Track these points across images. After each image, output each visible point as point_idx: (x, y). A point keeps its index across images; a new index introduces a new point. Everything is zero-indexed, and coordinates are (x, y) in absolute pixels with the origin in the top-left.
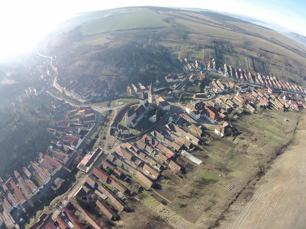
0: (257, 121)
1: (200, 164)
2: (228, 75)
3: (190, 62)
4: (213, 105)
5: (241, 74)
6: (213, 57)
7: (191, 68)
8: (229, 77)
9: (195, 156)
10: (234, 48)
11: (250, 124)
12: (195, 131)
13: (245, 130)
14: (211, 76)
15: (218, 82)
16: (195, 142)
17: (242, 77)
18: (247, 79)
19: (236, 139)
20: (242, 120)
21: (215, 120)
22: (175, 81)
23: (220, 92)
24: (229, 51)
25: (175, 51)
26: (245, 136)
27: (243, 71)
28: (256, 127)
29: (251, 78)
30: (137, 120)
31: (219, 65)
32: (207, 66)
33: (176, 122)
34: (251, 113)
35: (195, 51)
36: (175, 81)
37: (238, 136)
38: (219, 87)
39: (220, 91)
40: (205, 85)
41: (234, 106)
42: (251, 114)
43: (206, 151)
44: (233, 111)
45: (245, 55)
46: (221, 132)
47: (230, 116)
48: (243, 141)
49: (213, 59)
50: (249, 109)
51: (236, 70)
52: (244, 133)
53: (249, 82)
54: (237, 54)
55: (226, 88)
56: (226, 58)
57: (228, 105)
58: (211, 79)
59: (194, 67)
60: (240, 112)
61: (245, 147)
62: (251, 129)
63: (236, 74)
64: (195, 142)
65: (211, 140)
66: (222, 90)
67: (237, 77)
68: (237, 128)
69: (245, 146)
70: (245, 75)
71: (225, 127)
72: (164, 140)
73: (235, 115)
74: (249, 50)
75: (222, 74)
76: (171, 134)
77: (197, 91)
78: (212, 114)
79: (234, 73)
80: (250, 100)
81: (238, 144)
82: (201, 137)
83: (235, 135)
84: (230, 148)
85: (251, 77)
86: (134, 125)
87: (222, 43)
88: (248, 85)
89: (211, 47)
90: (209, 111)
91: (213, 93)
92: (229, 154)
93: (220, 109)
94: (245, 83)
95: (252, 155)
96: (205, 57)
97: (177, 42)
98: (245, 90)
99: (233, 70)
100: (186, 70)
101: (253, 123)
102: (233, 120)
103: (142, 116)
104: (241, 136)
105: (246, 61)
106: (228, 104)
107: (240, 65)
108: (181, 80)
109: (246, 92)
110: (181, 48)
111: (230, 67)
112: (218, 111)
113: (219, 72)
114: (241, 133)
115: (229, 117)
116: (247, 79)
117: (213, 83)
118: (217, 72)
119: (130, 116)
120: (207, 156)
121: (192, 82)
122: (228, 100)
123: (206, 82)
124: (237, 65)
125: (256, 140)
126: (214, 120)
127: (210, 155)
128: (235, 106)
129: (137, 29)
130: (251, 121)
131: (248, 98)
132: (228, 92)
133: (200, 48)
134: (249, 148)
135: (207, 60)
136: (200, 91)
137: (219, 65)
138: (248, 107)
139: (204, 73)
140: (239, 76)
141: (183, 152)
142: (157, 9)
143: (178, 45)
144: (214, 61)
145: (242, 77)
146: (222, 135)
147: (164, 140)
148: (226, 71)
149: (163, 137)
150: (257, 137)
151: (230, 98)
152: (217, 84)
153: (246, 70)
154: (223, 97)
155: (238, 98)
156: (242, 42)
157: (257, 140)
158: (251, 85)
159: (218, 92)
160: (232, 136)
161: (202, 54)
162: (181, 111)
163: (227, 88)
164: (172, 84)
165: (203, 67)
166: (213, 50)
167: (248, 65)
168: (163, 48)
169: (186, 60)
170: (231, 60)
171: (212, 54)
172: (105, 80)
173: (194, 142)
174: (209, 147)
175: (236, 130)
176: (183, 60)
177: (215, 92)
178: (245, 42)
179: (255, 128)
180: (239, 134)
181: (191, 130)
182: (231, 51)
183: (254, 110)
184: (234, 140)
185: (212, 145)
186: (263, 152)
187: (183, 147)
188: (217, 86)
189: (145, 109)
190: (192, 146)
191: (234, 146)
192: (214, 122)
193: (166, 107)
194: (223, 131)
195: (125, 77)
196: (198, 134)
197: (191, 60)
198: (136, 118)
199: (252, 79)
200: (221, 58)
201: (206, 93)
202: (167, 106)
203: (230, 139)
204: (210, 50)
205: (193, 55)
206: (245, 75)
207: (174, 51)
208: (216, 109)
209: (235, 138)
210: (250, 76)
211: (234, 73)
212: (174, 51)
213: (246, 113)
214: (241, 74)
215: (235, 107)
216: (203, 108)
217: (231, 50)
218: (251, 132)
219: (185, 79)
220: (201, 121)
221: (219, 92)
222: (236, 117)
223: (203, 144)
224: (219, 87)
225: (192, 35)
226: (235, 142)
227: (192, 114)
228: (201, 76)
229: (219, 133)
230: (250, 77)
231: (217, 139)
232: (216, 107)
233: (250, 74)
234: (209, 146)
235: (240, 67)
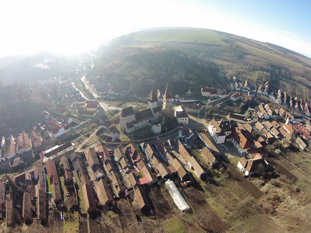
0: (306, 162)
1: (184, 211)
2: (281, 101)
3: (238, 81)
4: (249, 129)
5: (297, 104)
6: (267, 80)
7: (238, 87)
8: (282, 104)
9: (183, 194)
10: (292, 75)
11: (296, 165)
12: (207, 158)
13: (283, 171)
14: (259, 99)
15: (266, 106)
16: (198, 173)
17: (296, 106)
18: (303, 109)
19: (267, 185)
20: (285, 157)
21: (245, 150)
22: (212, 96)
23: (265, 118)
24: (286, 78)
25: (226, 69)
26: (284, 181)
27: (299, 101)
28: (304, 170)
29: (307, 109)
30: (135, 125)
31: (272, 90)
32: (257, 89)
33: (186, 141)
34: (300, 150)
35: (248, 72)
36: (212, 96)
37: (271, 180)
38: (267, 112)
39: (266, 117)
40: (249, 106)
41: (279, 137)
42: (300, 151)
43: (207, 193)
44: (275, 143)
45: (303, 84)
46: (245, 167)
47: (269, 147)
48: (278, 190)
49: (266, 82)
50: (299, 144)
51: (291, 98)
52: (283, 177)
53: (304, 113)
54: (295, 82)
55: (274, 113)
56: (282, 84)
57: (272, 135)
58: (258, 102)
59: (242, 87)
60: (286, 146)
61: (277, 201)
62: (296, 172)
63: (291, 101)
64: (198, 173)
65: (225, 177)
66: (268, 115)
67: (291, 105)
68: (274, 167)
69: (278, 199)
70: (301, 105)
71: (254, 162)
72: (152, 158)
73: (277, 148)
74: (308, 80)
75: (274, 100)
76: (166, 152)
77: (235, 112)
78: (244, 140)
79: (288, 101)
80: (302, 133)
81: (267, 193)
82: (213, 169)
83: (267, 178)
84: (249, 198)
85: (307, 108)
86: (129, 131)
87: (280, 68)
88: (302, 117)
89: (268, 70)
90: (241, 135)
91: (256, 118)
92: (243, 207)
93: (258, 136)
94: (299, 113)
95: (283, 217)
96: (258, 79)
97: (230, 61)
98: (299, 121)
99: (288, 98)
100: (230, 88)
101: (301, 163)
102: (271, 155)
103: (144, 122)
104: (277, 180)
105: (304, 91)
106: (272, 133)
107: (297, 93)
108: (220, 96)
109: (298, 124)
110: (234, 67)
111: (285, 93)
112: (254, 138)
113: (270, 96)
114: (278, 176)
115: (267, 149)
116: (303, 109)
117: (260, 106)
118: (268, 96)
119: (124, 117)
120: (204, 201)
121: (233, 101)
122: (272, 127)
123: (253, 104)
124: (294, 94)
125: (298, 191)
126: (244, 148)
127: (210, 201)
128: (281, 136)
129: (191, 43)
130: (297, 161)
131: (300, 131)
132: (275, 119)
133: (255, 69)
134: (282, 203)
135: (260, 83)
136: (240, 112)
137: (272, 90)
138: (297, 142)
139: (251, 94)
140: (294, 104)
141: (169, 183)
142: (220, 33)
143: (232, 63)
144: (267, 84)
145: (296, 106)
146: (247, 173)
147: (152, 158)
148: (279, 97)
149: (152, 152)
150: (300, 186)
151: (276, 125)
152: (265, 109)
153: (303, 101)
154: (267, 123)
155: (287, 130)
156: (302, 71)
157: (299, 192)
158: (307, 117)
159: (263, 117)
160: (262, 177)
161: (255, 76)
162: (202, 129)
163: (276, 114)
164: (207, 98)
165: (252, 88)
166: (269, 74)
167: (306, 95)
168: (215, 64)
169: (234, 78)
170: (288, 87)
171: (266, 76)
172: (130, 81)
173: (196, 173)
174: (218, 187)
175: (272, 170)
176: (232, 79)
177: (258, 117)
178: (305, 72)
179: (302, 171)
180: (276, 176)
181: (202, 156)
182: (289, 77)
183: (305, 147)
184: (263, 185)
185: (222, 185)
186: (303, 216)
187: (173, 177)
188: (264, 111)
189: (153, 115)
190: (189, 176)
191: (257, 194)
192: (242, 153)
193: (182, 119)
194: (249, 168)
195: (153, 81)
196: (209, 163)
197: (241, 80)
198: (134, 122)
199: (308, 110)
200: (276, 84)
201: (246, 114)
202: (185, 118)
203: (257, 182)
204: (265, 73)
205: (244, 75)
206: (301, 105)
207: (225, 69)
208: (252, 136)
209: (266, 182)
210: (306, 107)
211: (288, 101)
212: (225, 69)
213: (293, 148)
214: (297, 104)
215: (281, 139)
216: (233, 130)
217: (288, 76)
218: (295, 177)
219: (225, 96)
220: (225, 147)
221: (264, 117)
222: (277, 151)
223: (209, 180)
224: (267, 112)
225: (249, 56)
226: (264, 189)
227: (215, 136)
228: (248, 96)
229: (244, 168)
230: (306, 108)
231: (235, 177)
232: (253, 132)
233: (306, 105)
234: (217, 185)
235: (296, 96)
